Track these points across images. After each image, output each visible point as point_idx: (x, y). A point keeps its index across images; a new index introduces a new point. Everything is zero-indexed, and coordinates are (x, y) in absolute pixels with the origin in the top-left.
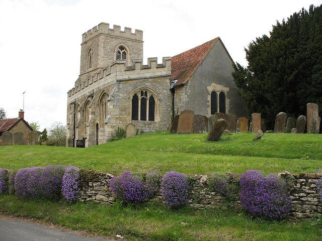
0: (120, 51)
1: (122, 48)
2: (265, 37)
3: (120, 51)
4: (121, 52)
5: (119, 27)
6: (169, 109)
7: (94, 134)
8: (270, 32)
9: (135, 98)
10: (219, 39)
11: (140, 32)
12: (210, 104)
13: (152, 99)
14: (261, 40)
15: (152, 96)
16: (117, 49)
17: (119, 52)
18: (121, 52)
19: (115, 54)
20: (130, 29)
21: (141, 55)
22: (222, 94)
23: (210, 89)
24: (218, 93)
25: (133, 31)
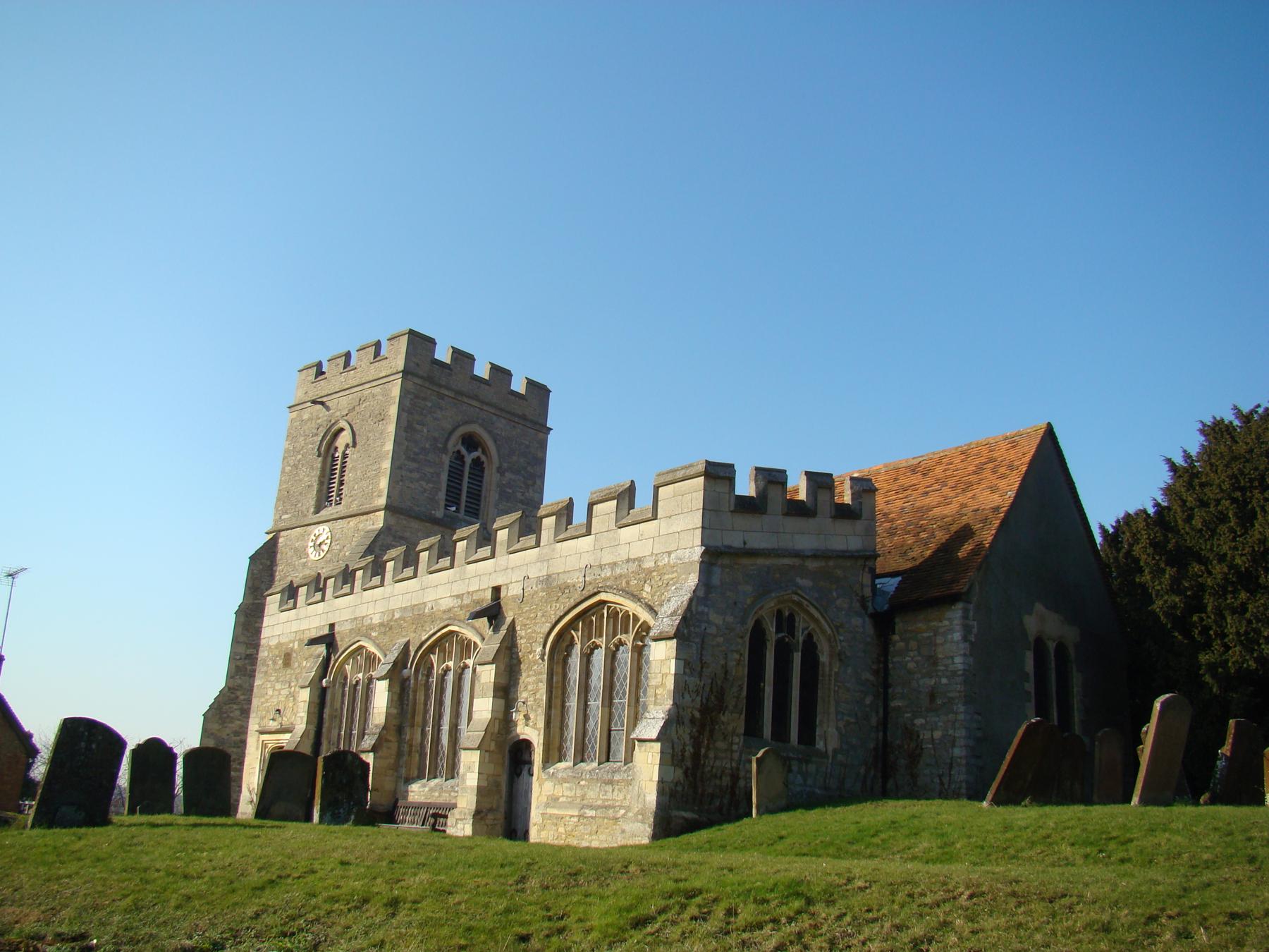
0: (464, 451)
1: (471, 442)
2: (1222, 420)
3: (464, 451)
4: (469, 459)
5: (432, 342)
6: (868, 701)
7: (497, 785)
8: (1169, 461)
9: (758, 638)
10: (757, 469)
11: (539, 392)
12: (1030, 686)
13: (810, 649)
14: (185, 949)
15: (810, 636)
16: (454, 444)
17: (459, 457)
18: (469, 459)
19: (446, 460)
20: (470, 359)
21: (538, 482)
22: (1061, 648)
23: (1031, 624)
24: (1051, 646)
25: (519, 385)
